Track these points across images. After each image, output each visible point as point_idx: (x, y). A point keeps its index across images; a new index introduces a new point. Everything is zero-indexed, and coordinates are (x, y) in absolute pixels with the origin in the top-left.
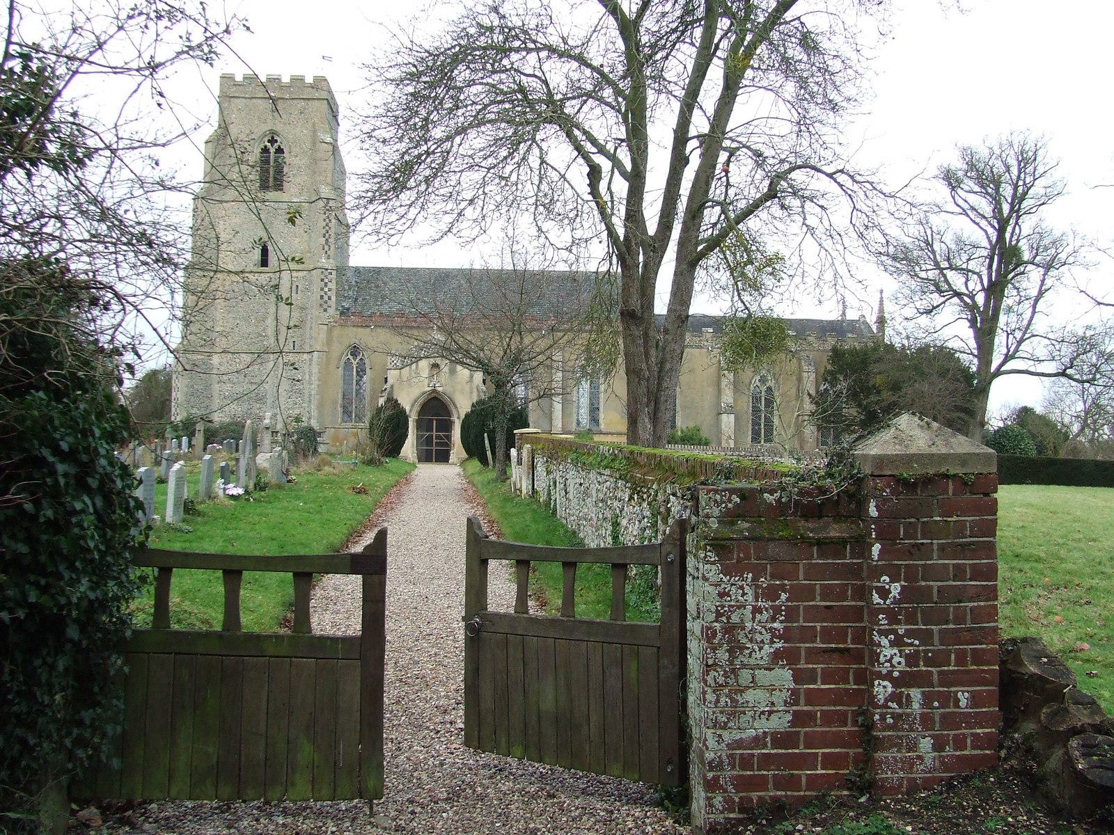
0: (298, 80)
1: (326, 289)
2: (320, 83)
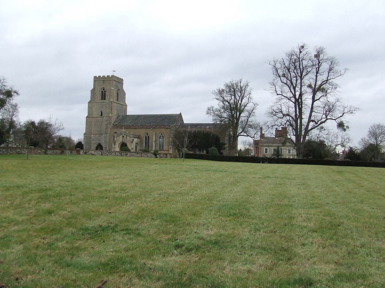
0: (108, 76)
1: (111, 121)
2: (122, 80)
